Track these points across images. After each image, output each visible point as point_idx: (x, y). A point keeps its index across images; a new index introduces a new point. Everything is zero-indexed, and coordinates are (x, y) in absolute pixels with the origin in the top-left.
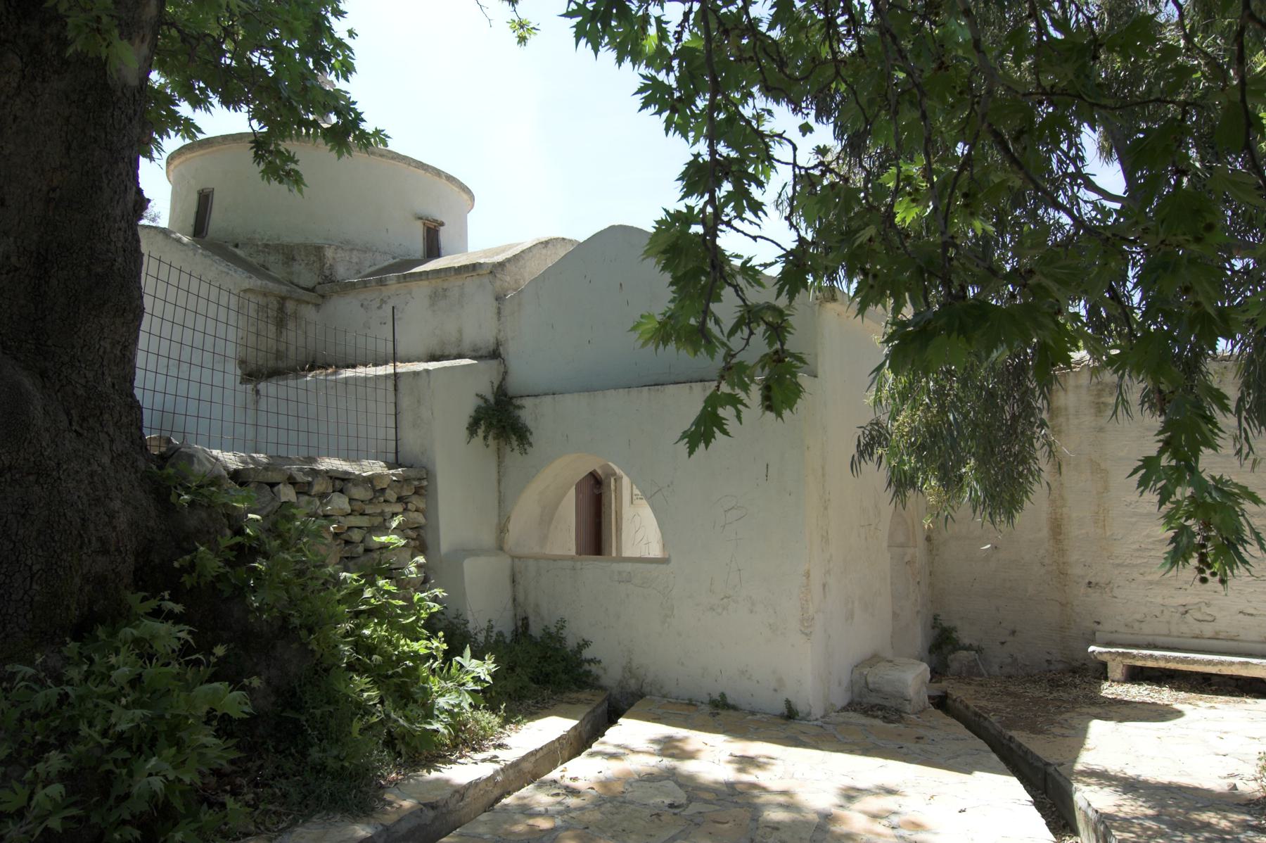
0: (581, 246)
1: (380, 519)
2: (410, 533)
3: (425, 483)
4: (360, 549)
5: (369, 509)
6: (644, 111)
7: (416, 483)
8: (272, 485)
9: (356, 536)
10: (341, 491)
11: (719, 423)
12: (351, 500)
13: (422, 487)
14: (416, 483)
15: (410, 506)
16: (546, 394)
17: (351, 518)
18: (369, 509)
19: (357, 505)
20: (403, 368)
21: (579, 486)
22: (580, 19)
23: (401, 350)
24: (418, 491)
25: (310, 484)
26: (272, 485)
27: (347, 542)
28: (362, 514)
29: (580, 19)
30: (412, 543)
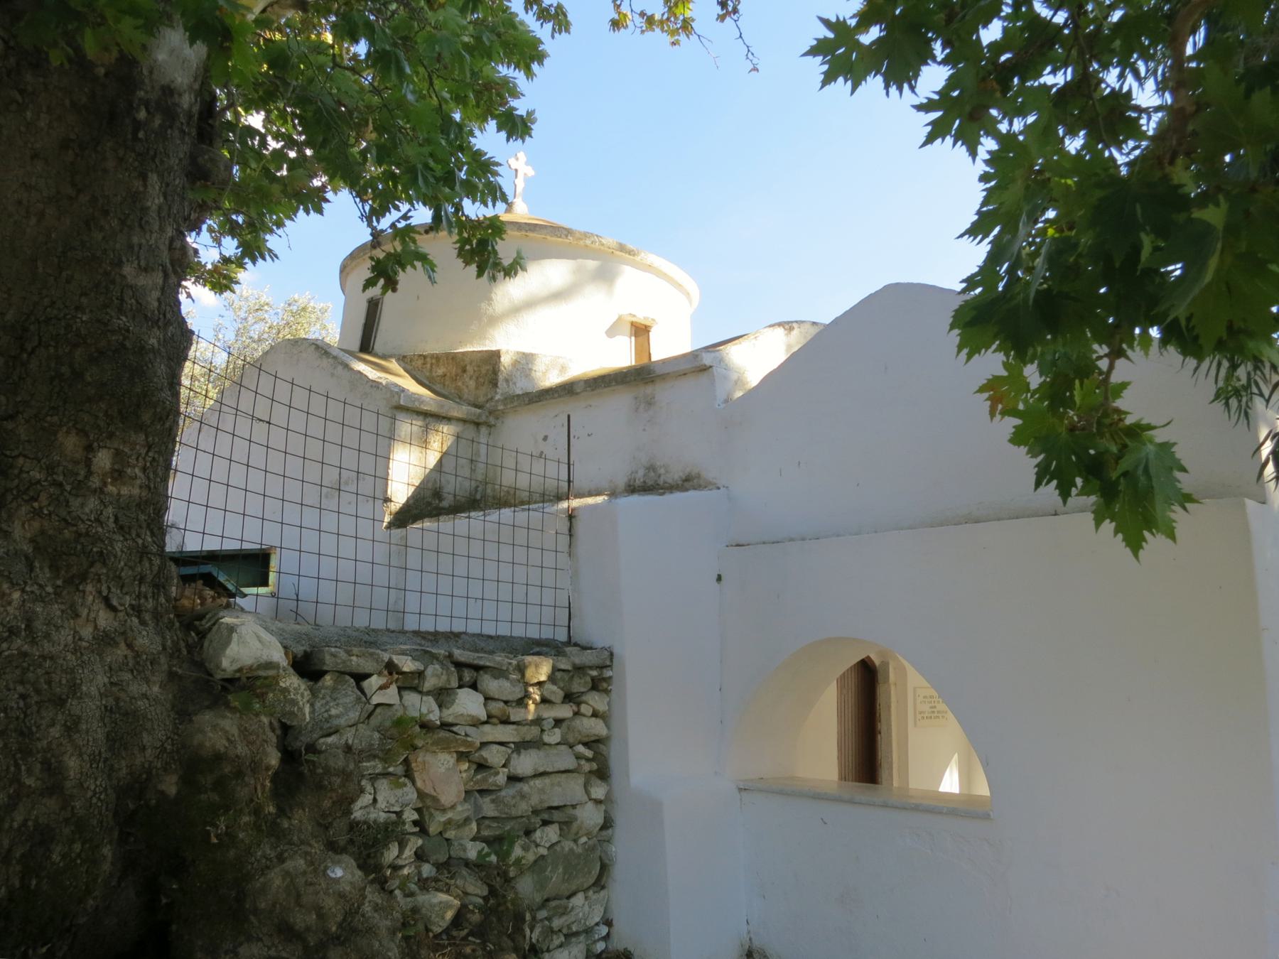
0: (828, 327)
1: (535, 731)
2: (580, 748)
3: (608, 673)
4: (501, 779)
5: (516, 714)
6: (810, 58)
7: (594, 673)
8: (360, 678)
9: (494, 756)
10: (474, 686)
11: (791, 329)
12: (488, 699)
13: (605, 680)
14: (594, 673)
15: (584, 709)
16: (792, 540)
17: (487, 728)
18: (516, 714)
19: (496, 707)
20: (575, 503)
21: (842, 680)
22: (938, 114)
23: (579, 481)
24: (598, 685)
25: (420, 674)
26: (360, 678)
27: (482, 766)
28: (506, 722)
29: (938, 114)
30: (587, 767)
